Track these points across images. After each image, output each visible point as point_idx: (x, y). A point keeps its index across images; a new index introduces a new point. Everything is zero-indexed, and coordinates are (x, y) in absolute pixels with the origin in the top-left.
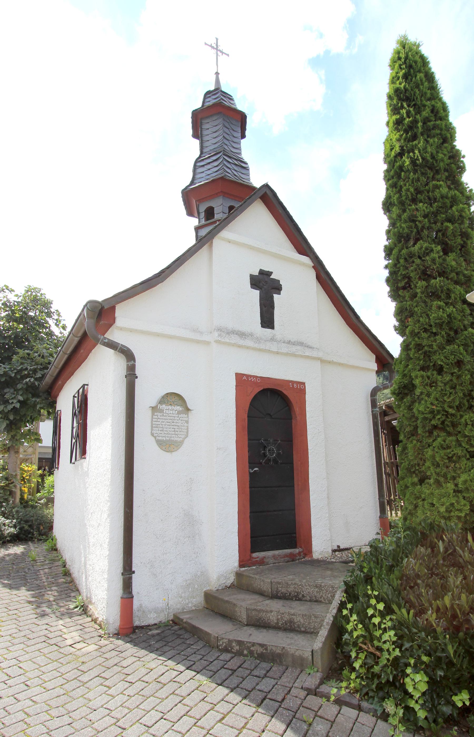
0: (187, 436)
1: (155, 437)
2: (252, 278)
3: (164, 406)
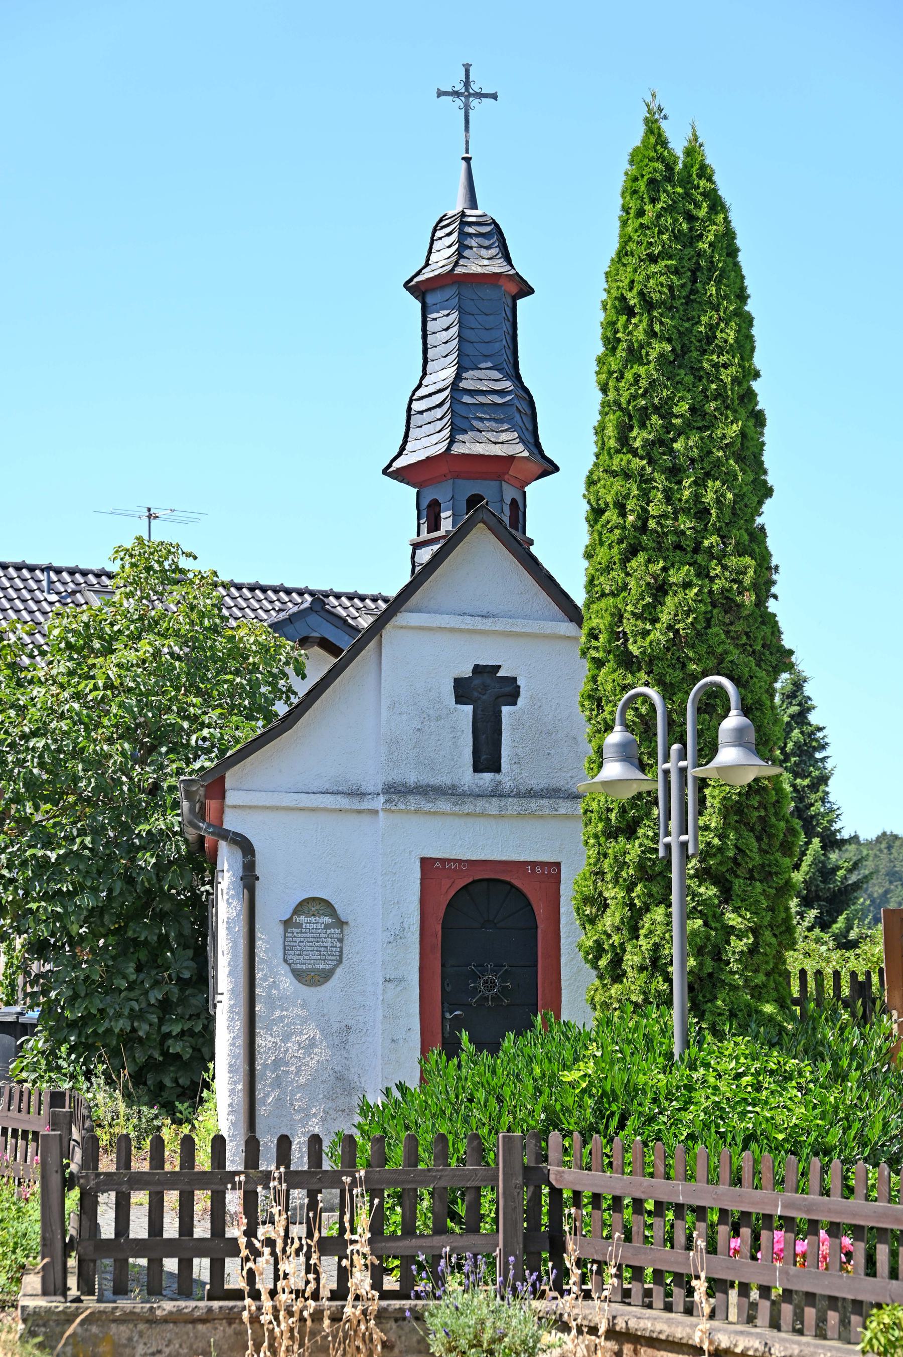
0: (340, 961)
1: (290, 965)
2: (459, 683)
3: (302, 918)
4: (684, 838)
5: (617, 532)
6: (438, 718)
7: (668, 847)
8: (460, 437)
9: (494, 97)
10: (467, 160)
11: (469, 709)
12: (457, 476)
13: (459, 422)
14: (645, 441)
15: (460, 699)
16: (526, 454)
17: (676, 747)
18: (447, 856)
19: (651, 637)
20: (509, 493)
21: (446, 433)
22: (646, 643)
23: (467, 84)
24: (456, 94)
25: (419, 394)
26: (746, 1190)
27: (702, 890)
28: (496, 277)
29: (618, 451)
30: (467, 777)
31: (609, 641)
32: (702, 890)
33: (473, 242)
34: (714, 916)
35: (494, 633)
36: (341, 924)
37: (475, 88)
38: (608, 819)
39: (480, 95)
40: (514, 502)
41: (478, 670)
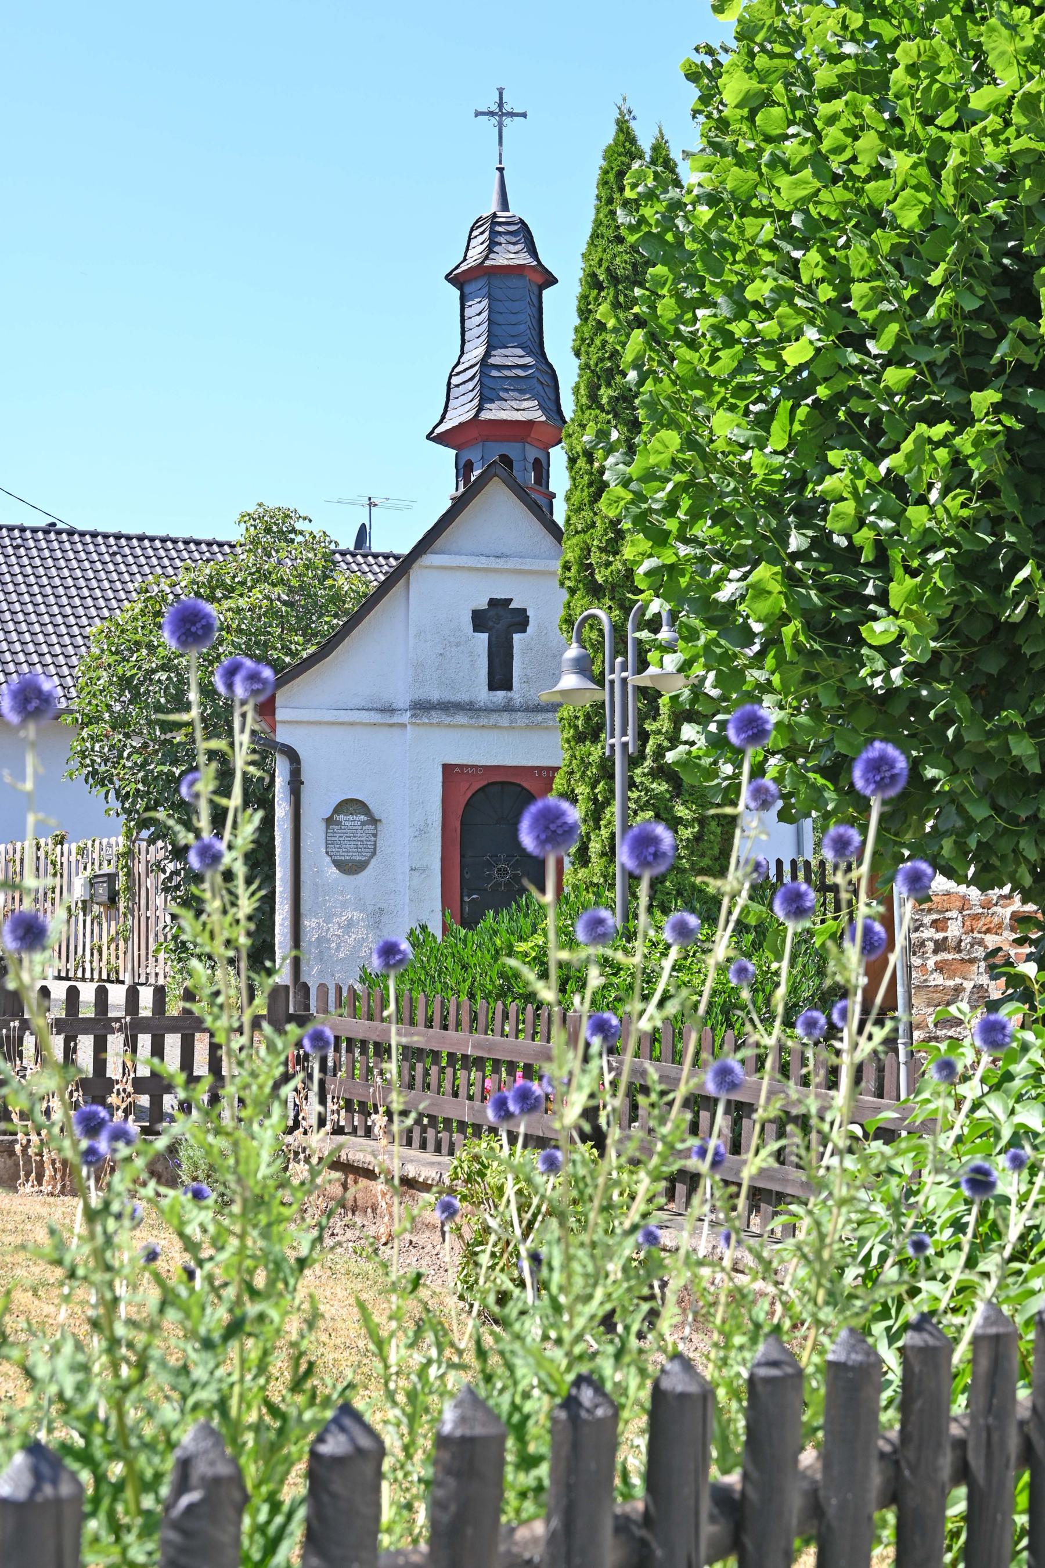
0: (374, 853)
4: (625, 739)
5: (586, 477)
6: (458, 645)
7: (612, 746)
8: (488, 406)
9: (524, 115)
10: (501, 170)
11: (484, 637)
12: (486, 439)
13: (487, 393)
14: (610, 397)
15: (478, 627)
16: (543, 418)
17: (619, 660)
18: (465, 762)
19: (613, 567)
20: (532, 453)
21: (476, 402)
22: (608, 572)
23: (501, 105)
24: (491, 114)
25: (457, 370)
26: (451, 1033)
27: (654, 786)
28: (518, 270)
29: (589, 408)
30: (482, 694)
31: (579, 572)
32: (654, 786)
33: (502, 240)
34: (666, 808)
35: (507, 571)
36: (374, 821)
37: (507, 108)
38: (576, 727)
39: (512, 114)
40: (537, 461)
41: (493, 602)
